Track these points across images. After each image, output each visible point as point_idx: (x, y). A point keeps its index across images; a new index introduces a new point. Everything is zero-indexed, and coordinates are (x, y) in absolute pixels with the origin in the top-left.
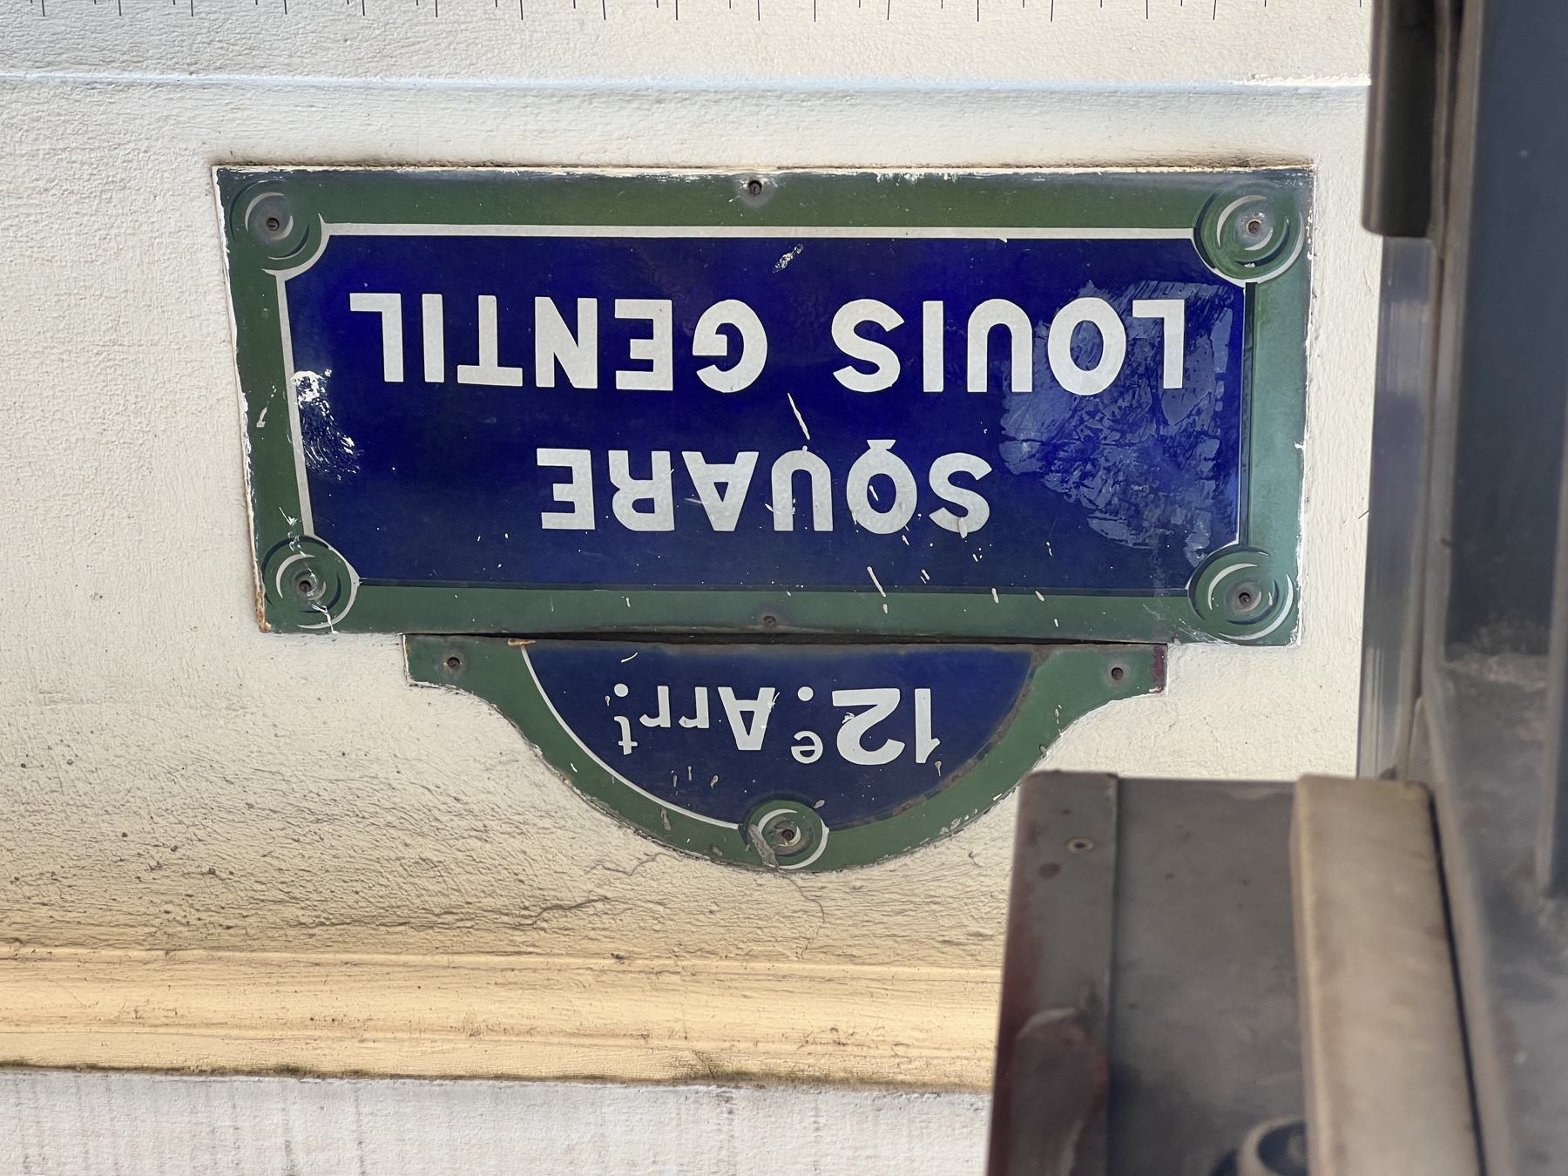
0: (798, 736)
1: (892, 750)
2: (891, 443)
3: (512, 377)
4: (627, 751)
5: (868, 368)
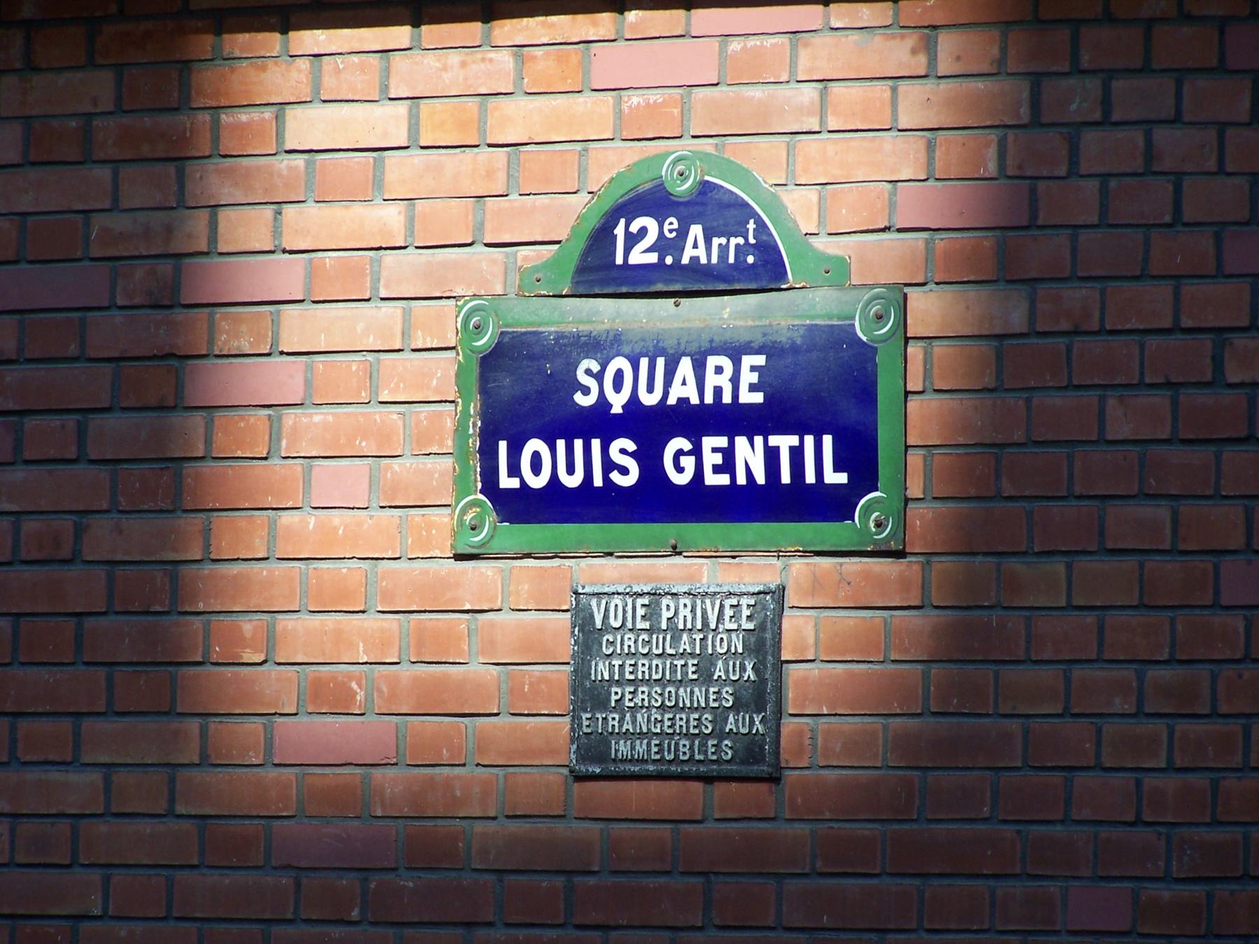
0: (674, 234)
1: (634, 228)
2: (613, 411)
3: (774, 440)
4: (752, 221)
5: (623, 451)
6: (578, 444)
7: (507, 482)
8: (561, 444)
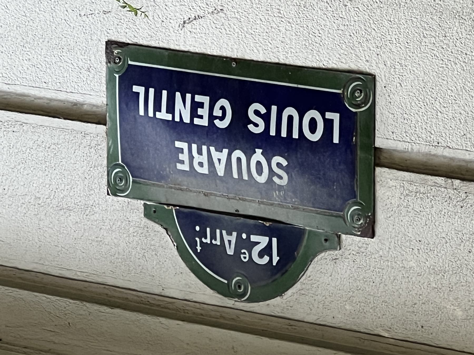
0: (243, 251)
1: (266, 259)
2: (261, 151)
3: (169, 117)
4: (199, 251)
5: (256, 125)
6: (284, 134)
7: (335, 117)
8: (295, 135)
